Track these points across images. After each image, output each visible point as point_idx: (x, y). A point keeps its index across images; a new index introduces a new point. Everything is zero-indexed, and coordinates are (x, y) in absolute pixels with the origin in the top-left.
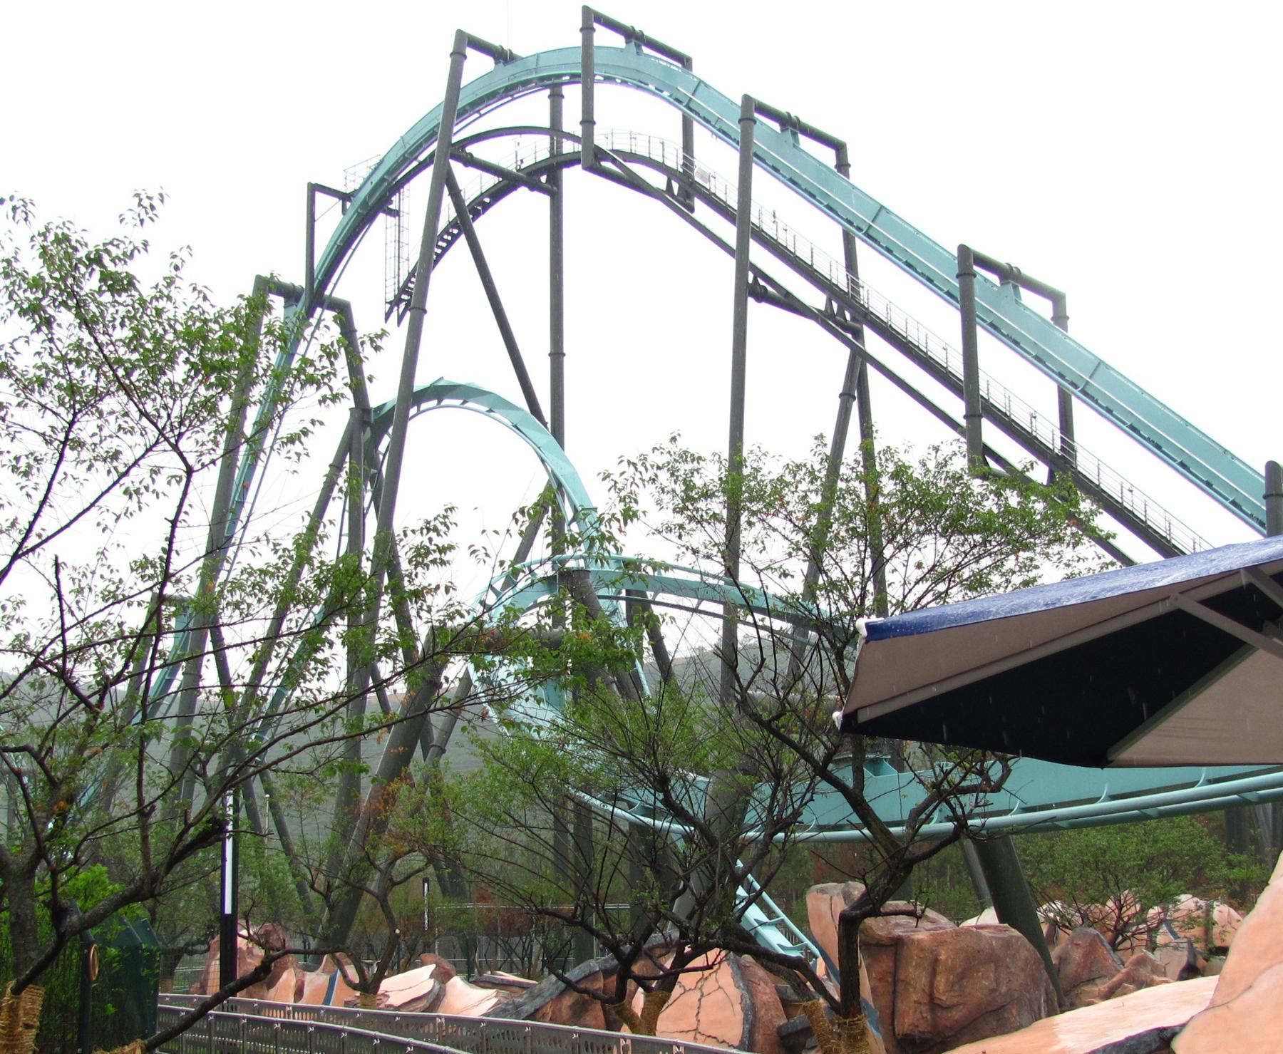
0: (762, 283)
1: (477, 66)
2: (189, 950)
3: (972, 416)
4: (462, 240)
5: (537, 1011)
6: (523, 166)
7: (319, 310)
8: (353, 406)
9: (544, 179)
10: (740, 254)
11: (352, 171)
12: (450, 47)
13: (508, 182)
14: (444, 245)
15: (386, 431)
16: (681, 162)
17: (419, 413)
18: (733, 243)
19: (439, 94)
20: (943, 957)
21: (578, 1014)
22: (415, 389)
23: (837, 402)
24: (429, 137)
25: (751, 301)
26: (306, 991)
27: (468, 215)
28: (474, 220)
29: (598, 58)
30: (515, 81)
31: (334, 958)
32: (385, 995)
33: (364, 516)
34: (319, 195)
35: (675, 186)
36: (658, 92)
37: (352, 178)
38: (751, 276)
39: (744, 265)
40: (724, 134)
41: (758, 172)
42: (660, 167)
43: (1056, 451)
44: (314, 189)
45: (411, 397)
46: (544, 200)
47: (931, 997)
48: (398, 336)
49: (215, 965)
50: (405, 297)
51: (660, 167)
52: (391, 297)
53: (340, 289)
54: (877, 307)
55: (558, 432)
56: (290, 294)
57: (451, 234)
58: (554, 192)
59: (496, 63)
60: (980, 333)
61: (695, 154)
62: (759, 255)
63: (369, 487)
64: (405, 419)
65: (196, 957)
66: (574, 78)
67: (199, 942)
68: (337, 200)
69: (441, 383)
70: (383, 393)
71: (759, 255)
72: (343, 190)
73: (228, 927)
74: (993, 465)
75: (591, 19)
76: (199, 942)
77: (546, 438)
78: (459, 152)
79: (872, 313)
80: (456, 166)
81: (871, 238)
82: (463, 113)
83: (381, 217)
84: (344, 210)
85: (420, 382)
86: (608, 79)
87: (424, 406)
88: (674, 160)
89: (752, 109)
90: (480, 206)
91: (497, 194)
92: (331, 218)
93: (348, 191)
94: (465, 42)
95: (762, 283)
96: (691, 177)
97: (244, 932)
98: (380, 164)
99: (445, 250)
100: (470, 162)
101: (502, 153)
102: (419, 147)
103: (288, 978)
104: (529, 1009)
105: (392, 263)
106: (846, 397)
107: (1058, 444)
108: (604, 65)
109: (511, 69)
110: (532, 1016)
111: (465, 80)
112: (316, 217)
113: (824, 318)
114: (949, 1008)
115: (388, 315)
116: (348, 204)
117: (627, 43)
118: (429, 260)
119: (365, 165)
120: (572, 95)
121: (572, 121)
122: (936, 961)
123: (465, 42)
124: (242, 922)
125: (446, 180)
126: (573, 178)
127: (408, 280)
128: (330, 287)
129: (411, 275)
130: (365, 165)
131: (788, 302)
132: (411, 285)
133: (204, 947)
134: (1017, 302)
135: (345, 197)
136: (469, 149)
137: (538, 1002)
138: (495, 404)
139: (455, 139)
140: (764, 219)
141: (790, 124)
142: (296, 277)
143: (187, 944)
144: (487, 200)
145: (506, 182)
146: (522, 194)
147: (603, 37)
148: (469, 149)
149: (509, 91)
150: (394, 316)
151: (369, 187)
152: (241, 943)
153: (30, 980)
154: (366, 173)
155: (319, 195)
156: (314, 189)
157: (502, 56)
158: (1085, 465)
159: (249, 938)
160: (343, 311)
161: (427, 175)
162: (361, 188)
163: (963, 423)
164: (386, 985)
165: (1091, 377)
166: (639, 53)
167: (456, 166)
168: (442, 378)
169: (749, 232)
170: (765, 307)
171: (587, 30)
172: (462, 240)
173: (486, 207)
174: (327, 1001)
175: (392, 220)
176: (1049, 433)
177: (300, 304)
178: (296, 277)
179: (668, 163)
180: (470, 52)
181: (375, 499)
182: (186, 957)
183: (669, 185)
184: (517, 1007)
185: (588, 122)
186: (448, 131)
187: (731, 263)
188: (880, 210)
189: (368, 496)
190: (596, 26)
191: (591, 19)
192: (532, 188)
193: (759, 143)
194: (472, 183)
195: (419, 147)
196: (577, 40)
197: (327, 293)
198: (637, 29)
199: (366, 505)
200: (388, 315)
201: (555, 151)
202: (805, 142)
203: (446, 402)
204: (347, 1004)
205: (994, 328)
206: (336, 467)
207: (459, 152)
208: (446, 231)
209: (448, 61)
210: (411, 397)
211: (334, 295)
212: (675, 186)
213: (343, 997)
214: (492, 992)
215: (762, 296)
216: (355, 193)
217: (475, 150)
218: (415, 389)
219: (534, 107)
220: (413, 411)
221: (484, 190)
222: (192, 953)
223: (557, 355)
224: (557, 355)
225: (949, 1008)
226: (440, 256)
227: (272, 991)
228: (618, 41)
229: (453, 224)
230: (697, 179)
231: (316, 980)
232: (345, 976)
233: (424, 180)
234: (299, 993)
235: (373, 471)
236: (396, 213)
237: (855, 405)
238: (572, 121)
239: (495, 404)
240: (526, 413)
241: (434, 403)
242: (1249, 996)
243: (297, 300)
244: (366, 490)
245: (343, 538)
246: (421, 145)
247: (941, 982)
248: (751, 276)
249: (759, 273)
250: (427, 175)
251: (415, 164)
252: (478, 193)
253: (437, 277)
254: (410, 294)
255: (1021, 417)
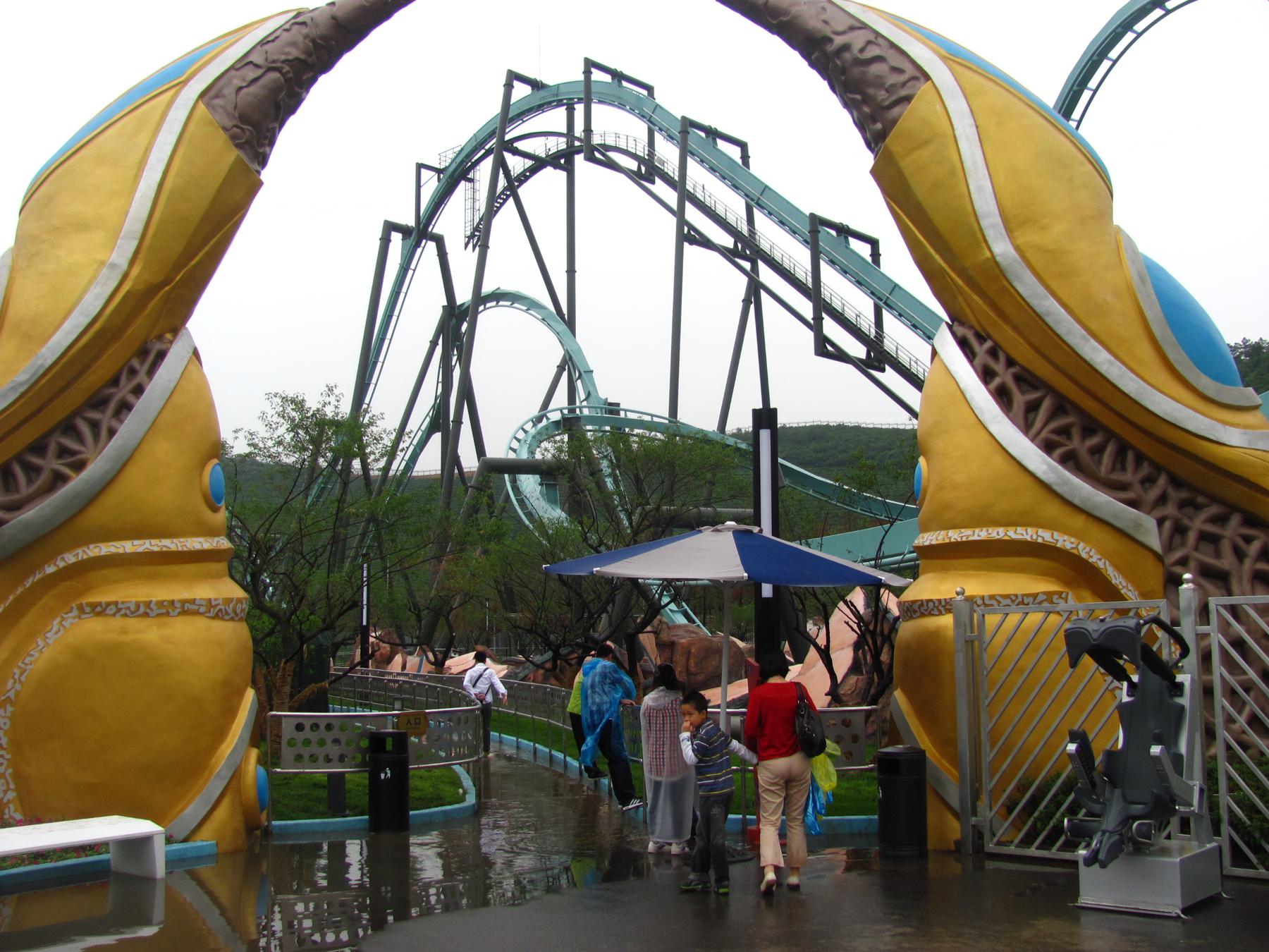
0: (692, 233)
1: (521, 91)
2: (344, 642)
3: (818, 319)
4: (511, 200)
5: (526, 676)
6: (550, 153)
7: (424, 241)
8: (446, 304)
9: (562, 161)
10: (679, 214)
11: (444, 154)
12: (503, 80)
13: (539, 164)
14: (501, 201)
15: (465, 320)
16: (646, 152)
17: (485, 309)
18: (674, 206)
19: (496, 109)
20: (693, 651)
21: (545, 680)
22: (482, 295)
23: (740, 305)
24: (491, 136)
25: (686, 245)
26: (408, 666)
27: (514, 184)
28: (519, 186)
29: (594, 88)
30: (542, 102)
31: (421, 648)
32: (449, 668)
33: (452, 371)
34: (423, 171)
35: (643, 169)
36: (632, 111)
37: (444, 159)
38: (686, 229)
39: (682, 221)
40: (670, 137)
41: (690, 161)
42: (634, 156)
43: (872, 337)
44: (420, 167)
45: (480, 299)
46: (562, 175)
47: (687, 668)
48: (472, 256)
49: (358, 652)
50: (477, 233)
51: (634, 156)
52: (468, 233)
53: (438, 228)
54: (765, 245)
55: (571, 323)
56: (405, 231)
57: (506, 195)
58: (569, 169)
59: (533, 90)
60: (823, 265)
61: (656, 149)
62: (693, 215)
63: (455, 352)
64: (476, 313)
65: (348, 647)
66: (580, 100)
67: (350, 639)
68: (434, 173)
69: (497, 292)
70: (463, 295)
71: (693, 215)
72: (438, 166)
73: (365, 633)
74: (829, 348)
75: (590, 65)
76: (350, 639)
77: (562, 327)
78: (509, 147)
79: (762, 250)
80: (508, 156)
81: (761, 207)
82: (513, 120)
83: (463, 183)
84: (439, 179)
85: (487, 289)
86: (600, 102)
87: (488, 305)
88: (642, 151)
89: (688, 125)
90: (524, 178)
91: (533, 170)
92: (431, 184)
93: (442, 167)
94: (513, 77)
95: (692, 233)
96: (653, 163)
97: (373, 634)
98: (462, 149)
99: (502, 204)
100: (516, 152)
101: (537, 147)
102: (485, 141)
103: (398, 659)
104: (522, 675)
105: (469, 212)
106: (746, 302)
107: (873, 331)
108: (598, 93)
109: (542, 93)
110: (523, 679)
111: (513, 101)
112: (423, 182)
113: (730, 255)
114: (696, 675)
115: (466, 245)
116: (442, 176)
117: (612, 79)
118: (491, 211)
119: (452, 151)
120: (579, 109)
121: (579, 130)
122: (689, 653)
123: (513, 77)
124: (372, 628)
125: (501, 164)
126: (579, 159)
127: (479, 223)
128: (431, 227)
129: (481, 220)
130: (452, 151)
131: (706, 243)
132: (481, 226)
133: (353, 641)
134: (847, 247)
135: (439, 171)
136: (515, 145)
137: (527, 671)
138: (531, 305)
139: (507, 137)
140: (697, 190)
141: (713, 134)
142: (410, 221)
143: (344, 640)
144: (528, 174)
145: (538, 164)
146: (548, 171)
147: (597, 75)
148: (515, 145)
149: (541, 108)
150: (471, 246)
151: (454, 166)
152: (371, 640)
153: (291, 659)
154: (452, 156)
155: (423, 171)
156: (420, 167)
157: (536, 85)
158: (889, 345)
159: (376, 638)
160: (439, 241)
161: (489, 161)
162: (449, 166)
163: (812, 322)
164: (448, 663)
165: (890, 294)
166: (620, 85)
167: (508, 156)
168: (499, 288)
169: (686, 196)
170: (696, 248)
171: (587, 73)
172: (511, 200)
173: (527, 178)
174: (419, 671)
175: (469, 185)
176: (867, 324)
177: (412, 238)
178: (410, 221)
179: (638, 153)
180: (516, 83)
181: (459, 359)
182: (343, 646)
183: (639, 168)
184: (516, 674)
185: (588, 130)
186: (503, 133)
187: (673, 221)
188: (764, 189)
189: (455, 358)
190: (593, 70)
191: (590, 65)
192: (555, 168)
193: (692, 144)
194: (516, 164)
195: (485, 141)
196: (581, 77)
197: (430, 230)
198: (619, 70)
199: (453, 364)
200: (466, 245)
201: (570, 145)
202: (721, 144)
203: (501, 303)
204: (429, 672)
205: (832, 262)
206: (434, 344)
207: (509, 147)
208: (502, 193)
209: (502, 90)
210: (480, 299)
211: (434, 231)
212: (643, 169)
213: (427, 669)
214: (505, 666)
215: (693, 241)
216: (447, 168)
217: (520, 145)
218: (482, 295)
219: (555, 119)
220: (481, 308)
221: (526, 167)
222: (346, 645)
223: (571, 271)
224: (571, 271)
225: (696, 675)
226: (499, 208)
227: (390, 666)
228: (607, 78)
229: (505, 189)
230: (656, 164)
231: (413, 660)
232: (427, 657)
233: (488, 164)
234: (404, 667)
235: (458, 343)
236: (471, 180)
237: (752, 307)
238: (579, 130)
239: (531, 305)
240: (551, 312)
241: (494, 303)
242: (814, 669)
243: (410, 235)
244: (454, 355)
245: (1078, 118)
246: (486, 140)
247: (692, 662)
248: (686, 229)
249: (691, 227)
250: (489, 161)
251: (483, 151)
252: (522, 169)
253: (497, 222)
254: (480, 231)
255: (850, 315)
